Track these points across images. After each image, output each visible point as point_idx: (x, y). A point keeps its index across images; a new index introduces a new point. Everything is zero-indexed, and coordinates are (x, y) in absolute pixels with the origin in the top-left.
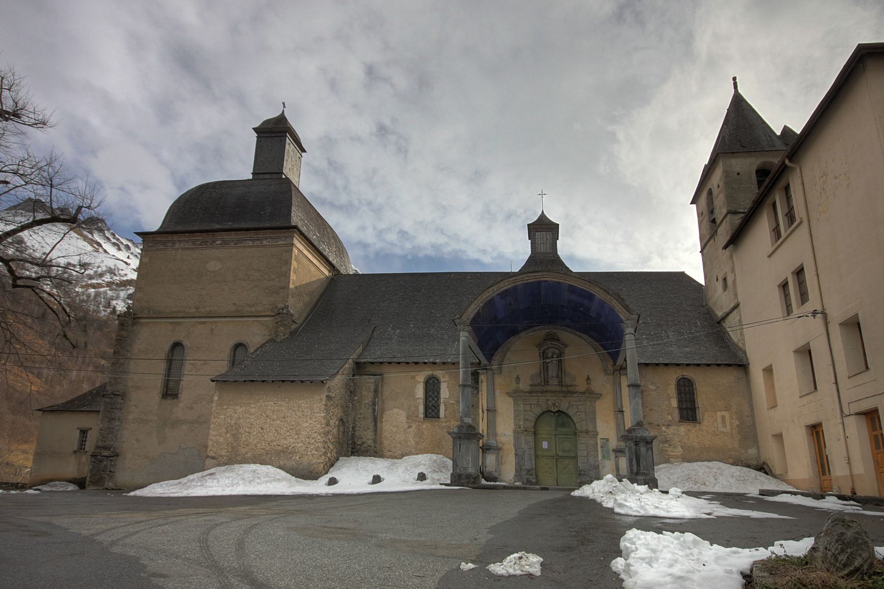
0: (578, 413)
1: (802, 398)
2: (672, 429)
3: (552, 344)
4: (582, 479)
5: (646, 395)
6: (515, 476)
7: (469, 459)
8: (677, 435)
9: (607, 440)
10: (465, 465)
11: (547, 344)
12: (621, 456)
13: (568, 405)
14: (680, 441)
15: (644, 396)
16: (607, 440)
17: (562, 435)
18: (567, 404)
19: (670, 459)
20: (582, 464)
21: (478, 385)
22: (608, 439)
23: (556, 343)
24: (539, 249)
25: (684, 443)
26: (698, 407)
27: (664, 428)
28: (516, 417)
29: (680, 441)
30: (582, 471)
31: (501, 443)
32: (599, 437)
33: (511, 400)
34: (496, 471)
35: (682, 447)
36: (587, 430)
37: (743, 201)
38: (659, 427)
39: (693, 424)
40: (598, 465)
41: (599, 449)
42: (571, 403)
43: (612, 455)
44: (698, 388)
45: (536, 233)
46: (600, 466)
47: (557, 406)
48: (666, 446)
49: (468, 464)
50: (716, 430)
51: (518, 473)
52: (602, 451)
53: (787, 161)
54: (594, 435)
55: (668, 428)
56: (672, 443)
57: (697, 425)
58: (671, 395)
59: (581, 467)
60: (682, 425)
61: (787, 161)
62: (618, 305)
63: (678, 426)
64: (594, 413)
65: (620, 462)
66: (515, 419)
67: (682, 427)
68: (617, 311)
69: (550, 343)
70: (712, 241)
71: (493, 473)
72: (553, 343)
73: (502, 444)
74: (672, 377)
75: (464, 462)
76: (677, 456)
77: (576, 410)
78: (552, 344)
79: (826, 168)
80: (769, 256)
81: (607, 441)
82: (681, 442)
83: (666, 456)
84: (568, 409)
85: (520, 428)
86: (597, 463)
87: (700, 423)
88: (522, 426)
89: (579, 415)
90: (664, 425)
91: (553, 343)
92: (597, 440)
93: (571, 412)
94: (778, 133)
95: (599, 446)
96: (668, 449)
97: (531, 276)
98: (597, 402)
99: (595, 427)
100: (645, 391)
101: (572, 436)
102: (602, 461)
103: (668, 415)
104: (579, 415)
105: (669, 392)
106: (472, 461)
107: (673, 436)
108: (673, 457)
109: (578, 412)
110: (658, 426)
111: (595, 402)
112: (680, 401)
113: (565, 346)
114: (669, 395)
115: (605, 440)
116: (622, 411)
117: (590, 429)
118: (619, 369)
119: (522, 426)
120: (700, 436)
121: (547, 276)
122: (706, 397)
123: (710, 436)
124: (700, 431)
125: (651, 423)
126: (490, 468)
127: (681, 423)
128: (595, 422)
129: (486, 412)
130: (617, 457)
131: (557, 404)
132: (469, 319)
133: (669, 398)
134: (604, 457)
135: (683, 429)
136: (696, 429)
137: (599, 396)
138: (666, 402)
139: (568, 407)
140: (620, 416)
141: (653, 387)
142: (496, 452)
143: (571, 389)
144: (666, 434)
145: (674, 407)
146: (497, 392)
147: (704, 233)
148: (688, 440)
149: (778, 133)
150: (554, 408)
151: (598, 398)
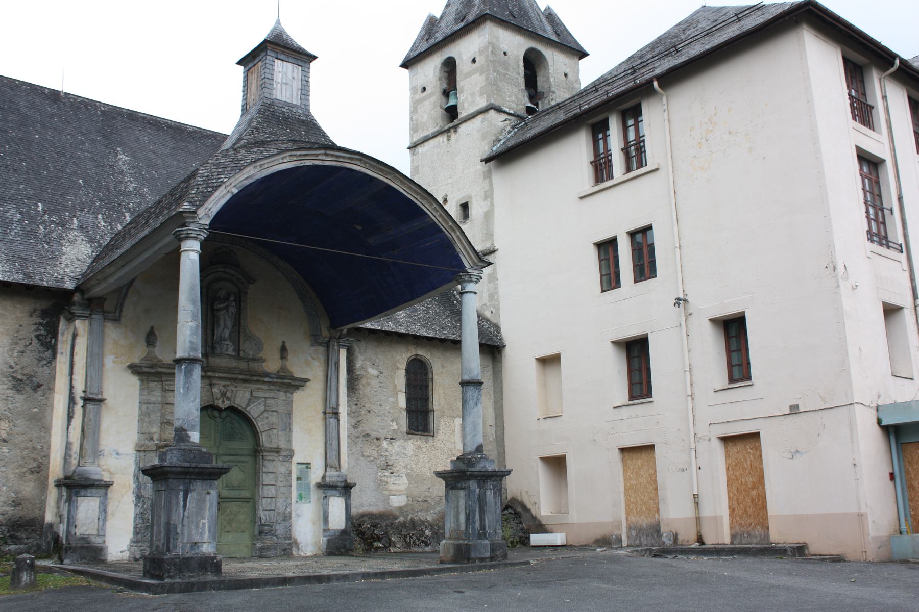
0: (265, 415)
1: (616, 409)
2: (397, 444)
3: (225, 272)
4: (265, 541)
5: (363, 385)
6: (133, 541)
7: (204, 524)
8: (403, 456)
9: (308, 465)
10: (196, 538)
11: (217, 272)
12: (332, 496)
13: (249, 397)
14: (405, 467)
15: (361, 386)
16: (308, 465)
17: (231, 455)
18: (248, 395)
19: (391, 497)
20: (267, 512)
21: (56, 340)
22: (309, 464)
23: (232, 272)
24: (278, 93)
25: (412, 469)
26: (433, 410)
27: (385, 444)
28: (144, 417)
29: (405, 467)
30: (266, 525)
31: (109, 471)
32: (296, 459)
33: (135, 381)
34: (98, 535)
35: (408, 475)
36: (278, 448)
37: (509, 97)
38: (377, 443)
39: (425, 437)
40: (290, 513)
41: (294, 483)
42: (254, 394)
43: (315, 495)
44: (435, 377)
45: (276, 60)
46: (293, 515)
47: (228, 399)
48: (386, 474)
49: (202, 534)
50: (453, 447)
51: (139, 536)
52: (298, 489)
53: (655, 84)
54: (287, 457)
55: (391, 443)
56: (395, 470)
57: (430, 438)
58: (398, 388)
59: (263, 518)
60: (410, 439)
61: (655, 84)
62: (463, 241)
63: (405, 440)
64: (289, 414)
65: (330, 507)
66: (141, 421)
67: (410, 442)
68: (458, 249)
69: (222, 270)
70: (442, 139)
71: (93, 539)
72: (227, 270)
73: (111, 473)
74: (401, 357)
75: (194, 531)
76: (400, 491)
77: (262, 408)
78: (225, 272)
79: (715, 115)
80: (581, 198)
81: (307, 467)
82: (407, 469)
83: (385, 492)
84: (248, 405)
85: (152, 439)
86: (288, 510)
87: (433, 436)
88: (156, 437)
89: (267, 418)
90: (385, 439)
91: (227, 270)
92: (290, 466)
93: (254, 411)
94: (543, 10)
95: (294, 477)
96: (389, 480)
97: (332, 155)
98: (294, 394)
99: (289, 441)
100: (361, 378)
101: (246, 459)
102: (298, 505)
103: (392, 421)
104: (267, 418)
105: (396, 383)
106: (210, 527)
107: (397, 457)
108: (395, 493)
109: (265, 411)
110: (378, 439)
111: (292, 394)
112: (409, 400)
113: (251, 280)
114: (395, 387)
115: (304, 466)
116: (336, 414)
117: (283, 445)
118: (338, 337)
119: (156, 437)
120: (432, 457)
121: (357, 163)
122: (444, 393)
123: (445, 458)
124: (433, 448)
125: (368, 435)
126: (85, 528)
127: (410, 436)
128: (290, 431)
129: (80, 403)
130: (326, 497)
131: (228, 394)
132: (209, 216)
133: (395, 392)
134: (300, 497)
135: (412, 444)
136: (427, 445)
137: (297, 384)
138: (392, 399)
139: (250, 400)
140: (333, 421)
141: (373, 372)
142: (102, 491)
143: (254, 365)
144: (387, 454)
145: (401, 408)
146: (109, 361)
147: (424, 121)
148: (416, 464)
149: (543, 10)
150: (223, 402)
151: (297, 387)
